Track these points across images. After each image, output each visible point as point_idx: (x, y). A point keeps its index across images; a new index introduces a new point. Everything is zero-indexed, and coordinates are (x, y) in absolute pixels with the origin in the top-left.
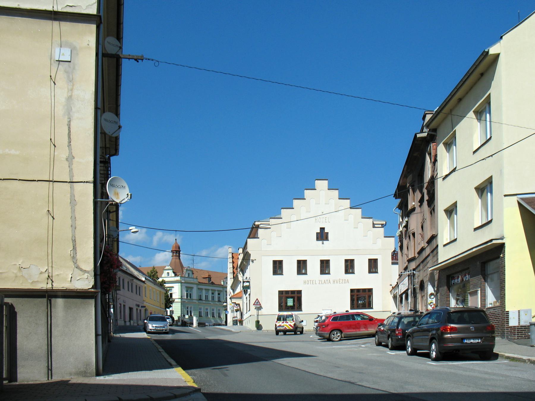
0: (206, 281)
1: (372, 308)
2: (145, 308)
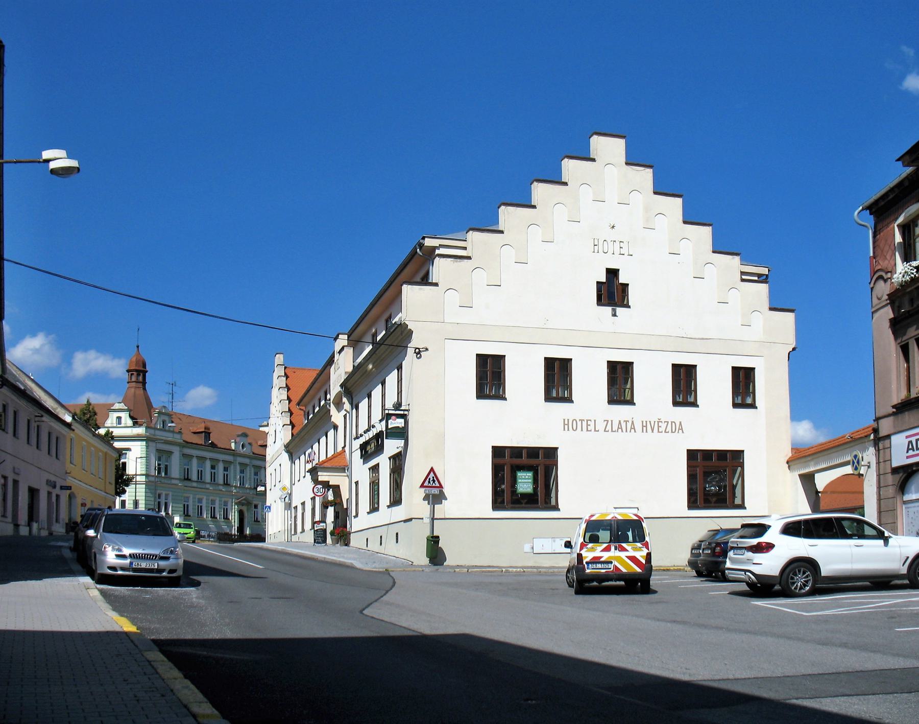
0: (200, 440)
1: (556, 508)
2: (68, 492)
